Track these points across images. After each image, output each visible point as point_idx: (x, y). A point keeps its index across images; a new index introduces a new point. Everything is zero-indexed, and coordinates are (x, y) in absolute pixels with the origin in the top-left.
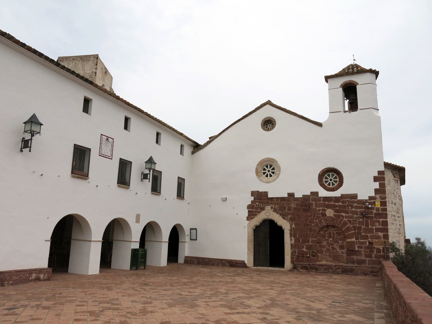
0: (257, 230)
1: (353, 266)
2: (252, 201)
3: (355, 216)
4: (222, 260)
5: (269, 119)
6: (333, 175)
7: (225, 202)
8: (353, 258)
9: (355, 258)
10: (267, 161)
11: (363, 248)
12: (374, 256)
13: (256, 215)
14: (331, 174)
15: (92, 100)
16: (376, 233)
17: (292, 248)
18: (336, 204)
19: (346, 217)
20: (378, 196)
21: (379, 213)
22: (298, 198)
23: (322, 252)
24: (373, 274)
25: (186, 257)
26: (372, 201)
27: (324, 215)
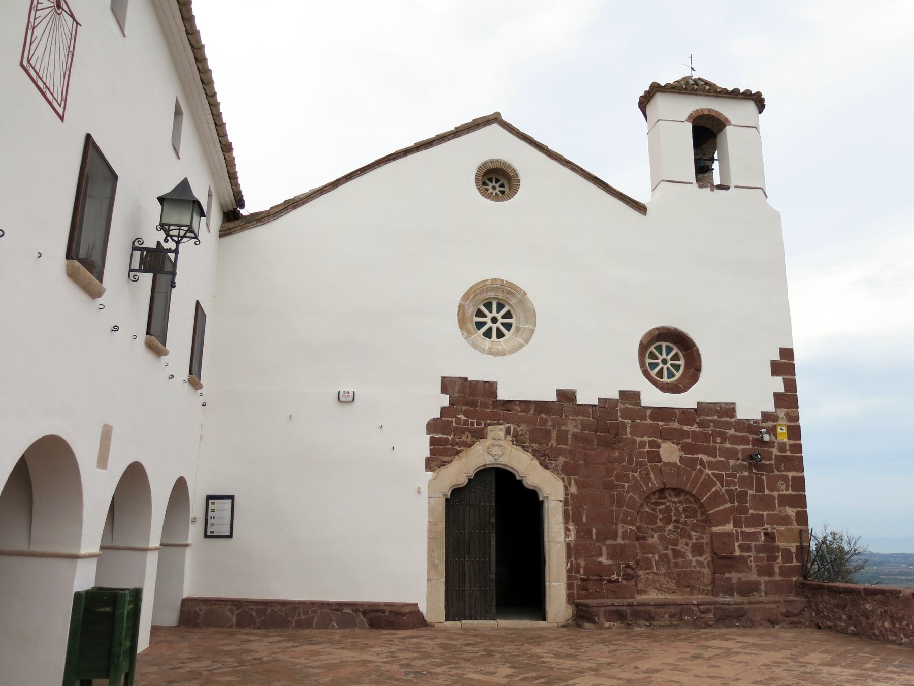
0: (456, 501)
1: (743, 603)
2: (443, 409)
3: (732, 462)
4: (339, 606)
5: (498, 166)
6: (669, 350)
7: (347, 408)
8: (730, 579)
9: (734, 577)
10: (492, 289)
11: (753, 549)
12: (777, 570)
13: (458, 452)
14: (664, 344)
16: (781, 508)
17: (569, 557)
18: (685, 428)
19: (711, 465)
20: (781, 413)
21: (785, 457)
23: (648, 565)
24: (791, 619)
25: (185, 602)
26: (770, 424)
27: (655, 457)
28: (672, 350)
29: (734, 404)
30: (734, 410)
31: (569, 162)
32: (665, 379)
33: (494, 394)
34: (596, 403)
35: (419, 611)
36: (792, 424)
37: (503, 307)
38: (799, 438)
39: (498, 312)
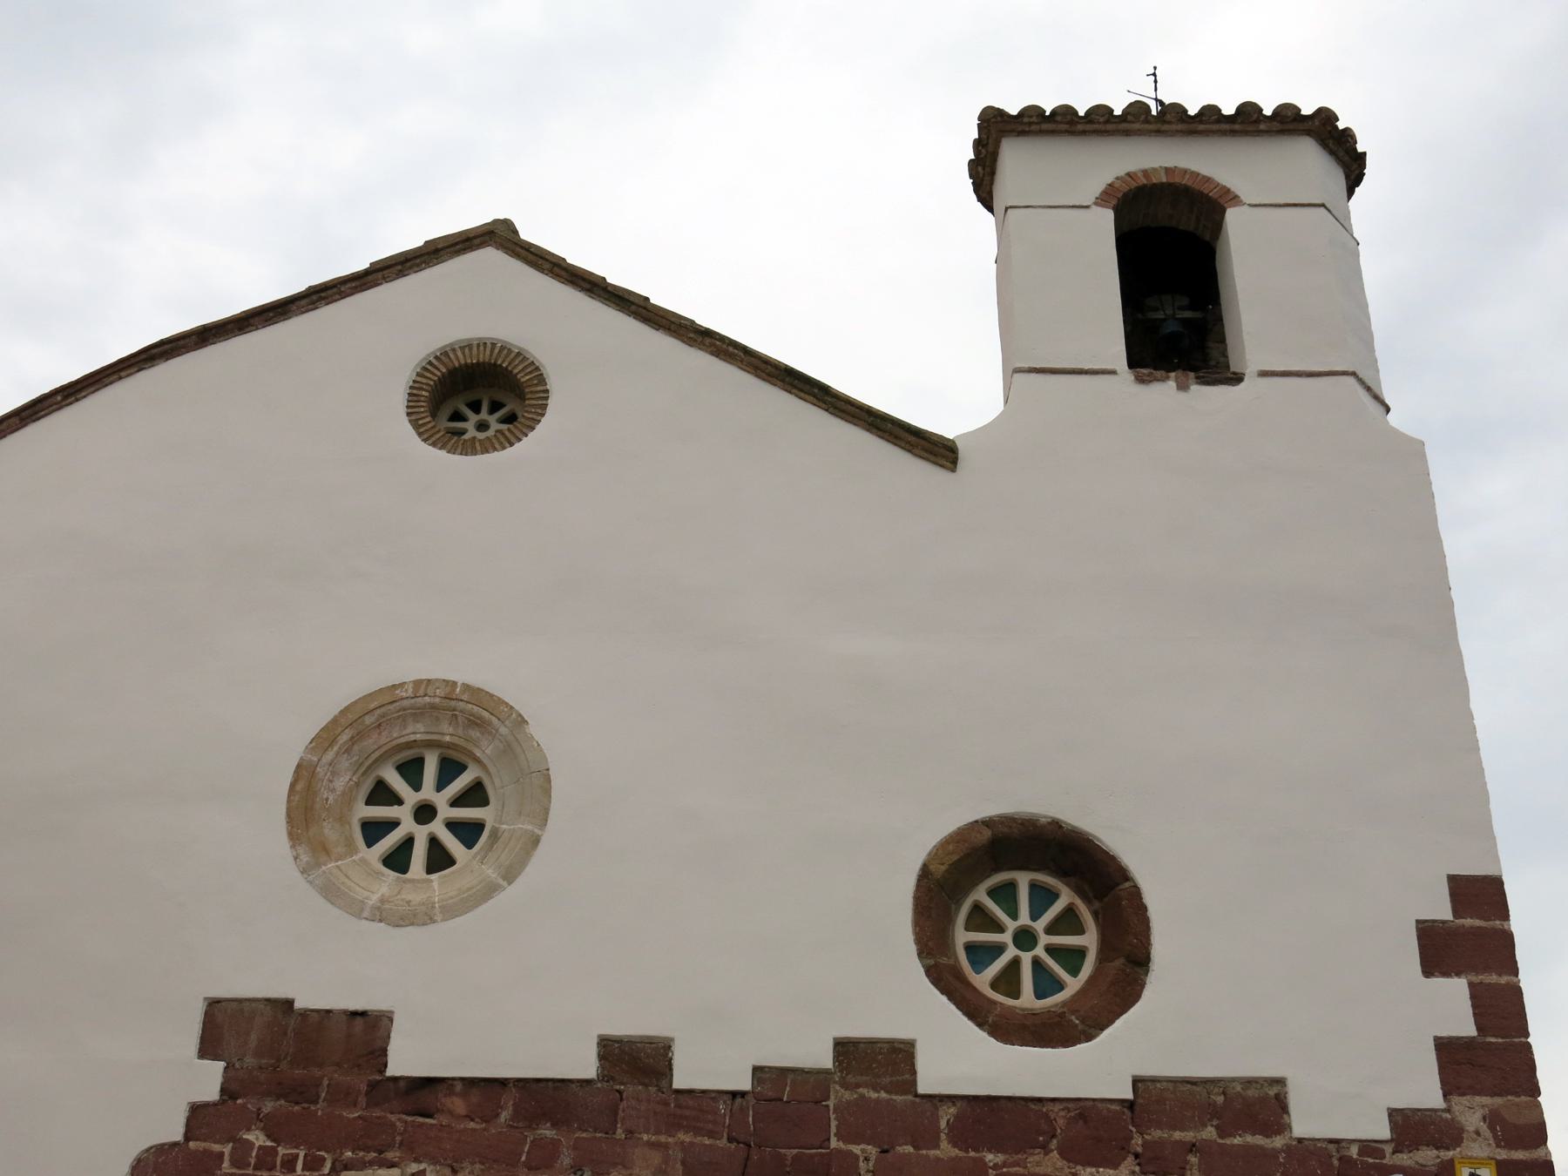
5: (484, 357)
6: (1042, 898)
10: (418, 713)
14: (1023, 880)
20: (1471, 1113)
28: (1035, 896)
29: (1280, 1082)
30: (1281, 1105)
31: (707, 333)
32: (1027, 999)
33: (379, 1056)
34: (745, 1084)
36: (1519, 1155)
37: (462, 768)
39: (441, 785)
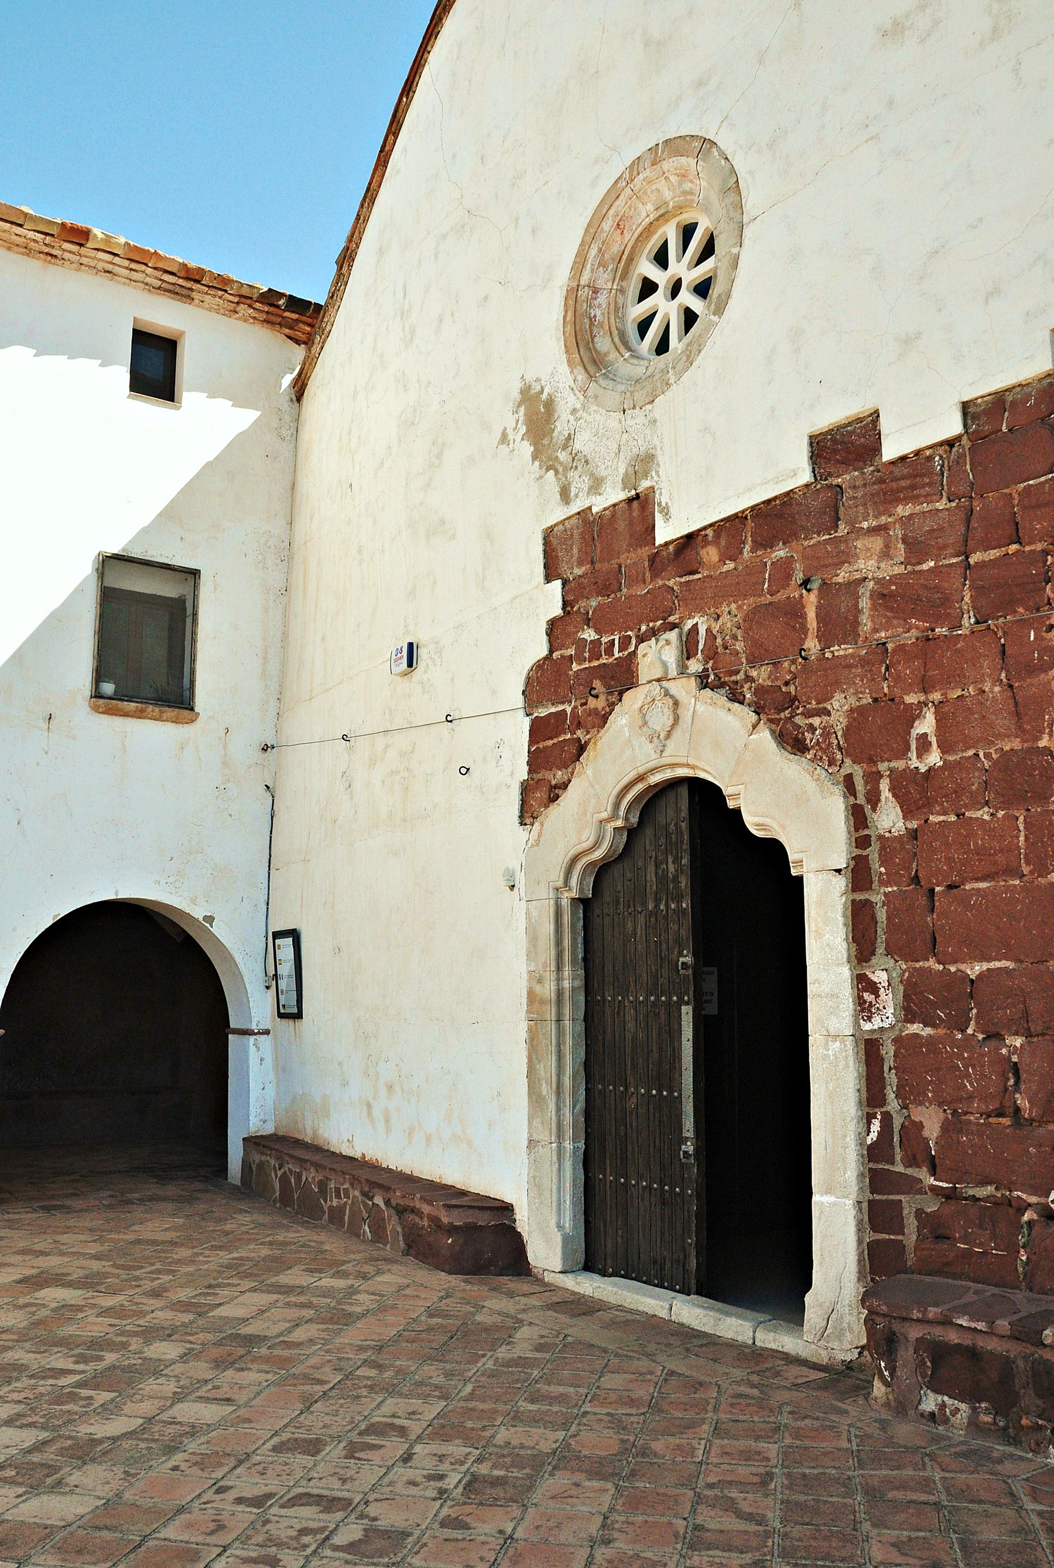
15: (182, 334)
22: (915, 464)
35: (513, 1230)
38: (310, 303)
